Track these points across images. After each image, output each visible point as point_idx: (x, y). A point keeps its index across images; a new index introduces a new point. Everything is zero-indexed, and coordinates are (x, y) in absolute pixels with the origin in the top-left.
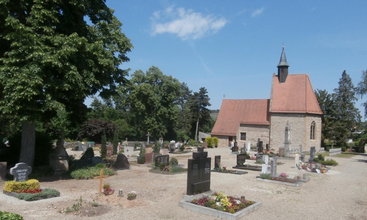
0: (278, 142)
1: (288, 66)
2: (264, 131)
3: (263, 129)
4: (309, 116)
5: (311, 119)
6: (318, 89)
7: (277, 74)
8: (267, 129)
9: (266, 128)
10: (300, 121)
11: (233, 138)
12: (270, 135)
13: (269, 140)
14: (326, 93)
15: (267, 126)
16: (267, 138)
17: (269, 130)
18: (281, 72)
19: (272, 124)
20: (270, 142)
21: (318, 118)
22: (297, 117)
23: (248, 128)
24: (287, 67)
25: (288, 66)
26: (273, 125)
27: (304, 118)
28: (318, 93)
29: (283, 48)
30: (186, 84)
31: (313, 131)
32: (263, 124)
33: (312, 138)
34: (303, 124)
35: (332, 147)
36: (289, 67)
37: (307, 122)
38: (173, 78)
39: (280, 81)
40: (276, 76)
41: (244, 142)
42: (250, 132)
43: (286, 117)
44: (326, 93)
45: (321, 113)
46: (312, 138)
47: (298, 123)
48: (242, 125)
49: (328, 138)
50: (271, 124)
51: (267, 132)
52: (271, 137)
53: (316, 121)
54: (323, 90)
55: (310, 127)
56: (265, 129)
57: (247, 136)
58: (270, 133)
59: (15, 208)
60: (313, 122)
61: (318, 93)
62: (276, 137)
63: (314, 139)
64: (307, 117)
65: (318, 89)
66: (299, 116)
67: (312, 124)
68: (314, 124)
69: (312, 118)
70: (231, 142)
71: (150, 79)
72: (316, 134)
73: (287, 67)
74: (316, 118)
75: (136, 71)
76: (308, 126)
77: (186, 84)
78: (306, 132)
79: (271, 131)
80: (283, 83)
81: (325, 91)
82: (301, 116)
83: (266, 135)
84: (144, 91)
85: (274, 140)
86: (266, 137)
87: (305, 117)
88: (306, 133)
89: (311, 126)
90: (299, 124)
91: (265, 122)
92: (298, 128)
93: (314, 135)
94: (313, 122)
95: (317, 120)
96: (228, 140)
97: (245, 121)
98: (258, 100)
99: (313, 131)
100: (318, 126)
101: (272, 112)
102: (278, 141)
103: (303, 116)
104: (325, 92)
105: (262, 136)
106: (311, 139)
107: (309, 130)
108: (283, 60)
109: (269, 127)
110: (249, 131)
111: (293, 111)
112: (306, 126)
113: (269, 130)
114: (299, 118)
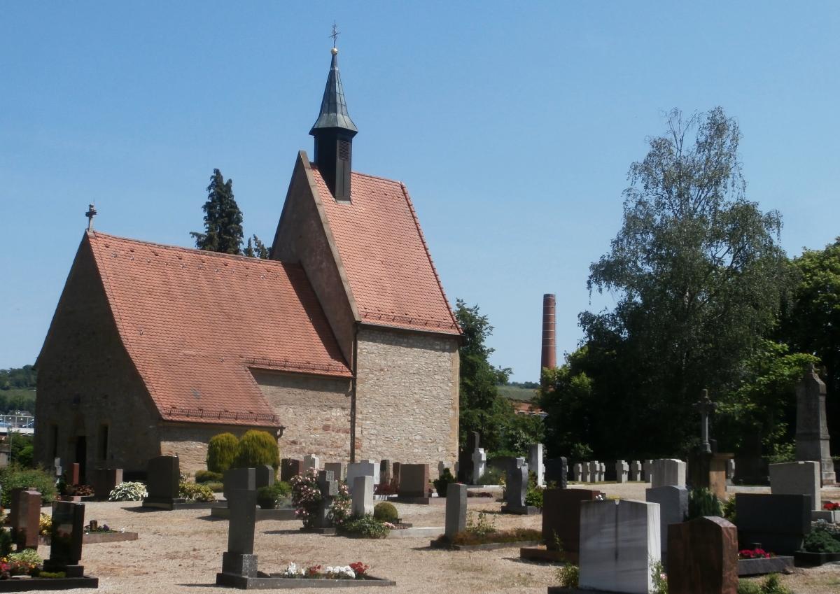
1: (353, 133)
3: (329, 395)
9: (338, 391)
12: (353, 422)
16: (343, 435)
18: (738, 496)
19: (360, 374)
25: (353, 133)
29: (334, 54)
35: (552, 369)
36: (355, 140)
39: (337, 191)
45: (455, 332)
59: (116, 557)
62: (373, 431)
79: (357, 402)
85: (365, 444)
86: (338, 431)
101: (365, 321)
102: (379, 449)
111: (402, 320)
113: (350, 398)
114: (438, 353)
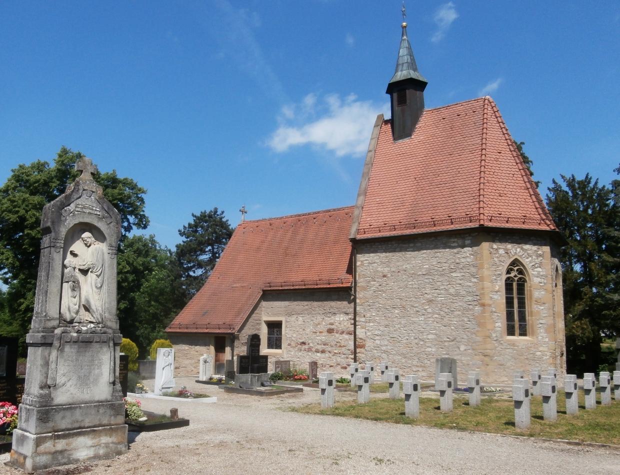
0: (385, 352)
2: (336, 311)
4: (493, 240)
5: (501, 252)
6: (563, 177)
7: (388, 116)
8: (345, 303)
10: (458, 261)
11: (227, 341)
12: (355, 325)
13: (352, 343)
14: (591, 185)
15: (345, 293)
16: (347, 337)
17: (352, 305)
19: (361, 282)
20: (358, 350)
21: (535, 248)
22: (445, 248)
23: (286, 303)
24: (420, 85)
26: (364, 289)
27: (475, 248)
28: (566, 189)
30: (223, 212)
31: (516, 301)
32: (331, 286)
33: (517, 331)
34: (473, 276)
37: (486, 266)
38: (120, 176)
40: (386, 122)
41: (277, 354)
42: (293, 318)
43: (409, 254)
44: (591, 185)
45: (544, 227)
46: (517, 331)
47: (452, 271)
48: (269, 294)
49: (18, 285)
50: (358, 285)
51: (347, 314)
52: (360, 333)
53: (526, 261)
54: (580, 177)
55: (501, 285)
56: (339, 303)
57: (283, 333)
58: (355, 319)
60: (515, 262)
61: (566, 189)
63: (523, 333)
64: (485, 245)
65: (563, 177)
66: (454, 241)
67: (508, 272)
68: (520, 272)
69: (509, 246)
70: (219, 354)
71: (42, 181)
72: (531, 314)
73: (420, 85)
74: (527, 247)
75: (20, 166)
76: (492, 282)
77: (223, 212)
78: (483, 305)
79: (358, 309)
80: (407, 140)
81: (588, 180)
82: (460, 242)
83: (342, 327)
84: (10, 211)
85: (369, 344)
86: (342, 333)
87: (475, 243)
88: (483, 312)
89: (508, 278)
90: (454, 275)
91: (341, 278)
92: (452, 291)
93: (522, 318)
94: (515, 262)
95: (529, 256)
96: (212, 348)
97: (279, 280)
98: (334, 210)
99: (516, 301)
100: (536, 280)
102: (384, 348)
103: (468, 242)
104: (589, 182)
105: (330, 331)
106: (511, 331)
107: (500, 299)
108: (403, 64)
109: (351, 295)
110: (290, 314)
112: (481, 279)
114: (455, 250)
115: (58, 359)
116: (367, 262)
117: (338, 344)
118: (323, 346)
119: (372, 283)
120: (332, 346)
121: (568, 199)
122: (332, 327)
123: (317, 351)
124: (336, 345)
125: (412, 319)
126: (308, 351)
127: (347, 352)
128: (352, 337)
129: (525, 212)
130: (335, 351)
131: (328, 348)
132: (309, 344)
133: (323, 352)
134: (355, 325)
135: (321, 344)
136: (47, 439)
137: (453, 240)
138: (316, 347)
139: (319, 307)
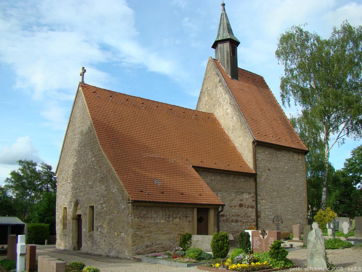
13: (254, 214)
105: (241, 205)
115: (62, 154)
116: (260, 158)
117: (246, 215)
118: (236, 217)
119: (263, 173)
120: (242, 217)
121: (20, 175)
122: (242, 202)
123: (232, 221)
124: (245, 216)
125: (282, 199)
126: (226, 222)
127: (251, 221)
128: (254, 210)
129: (202, 160)
130: (245, 221)
131: (239, 218)
132: (226, 216)
133: (237, 221)
134: (256, 201)
135: (234, 216)
136: (45, 28)
137: (295, 155)
138: (232, 219)
139: (233, 186)
